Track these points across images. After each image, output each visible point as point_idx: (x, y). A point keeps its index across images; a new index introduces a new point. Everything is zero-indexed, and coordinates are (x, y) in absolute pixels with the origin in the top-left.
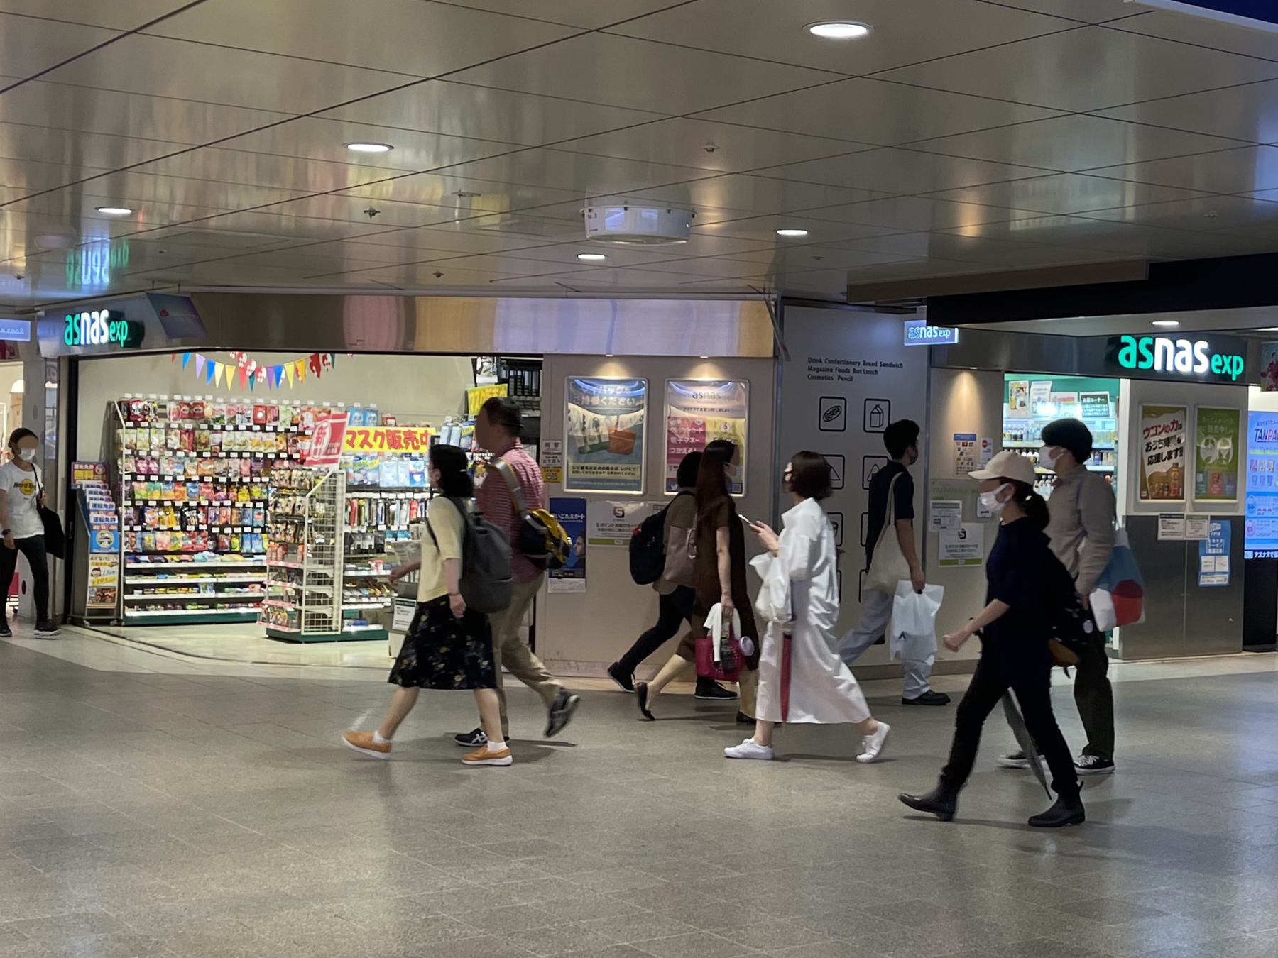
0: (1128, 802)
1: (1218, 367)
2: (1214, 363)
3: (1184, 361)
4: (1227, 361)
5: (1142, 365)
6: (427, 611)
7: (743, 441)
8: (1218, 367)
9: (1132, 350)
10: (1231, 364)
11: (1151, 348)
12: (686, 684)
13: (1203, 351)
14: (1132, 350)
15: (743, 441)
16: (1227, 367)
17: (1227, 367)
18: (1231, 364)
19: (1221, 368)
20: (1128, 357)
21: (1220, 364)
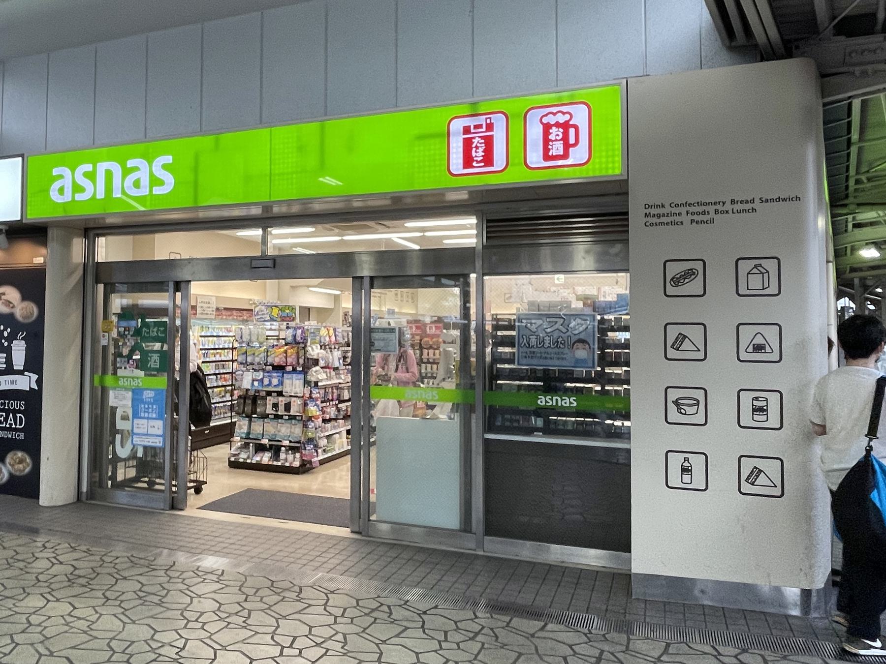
11: (91, 176)
20: (61, 190)
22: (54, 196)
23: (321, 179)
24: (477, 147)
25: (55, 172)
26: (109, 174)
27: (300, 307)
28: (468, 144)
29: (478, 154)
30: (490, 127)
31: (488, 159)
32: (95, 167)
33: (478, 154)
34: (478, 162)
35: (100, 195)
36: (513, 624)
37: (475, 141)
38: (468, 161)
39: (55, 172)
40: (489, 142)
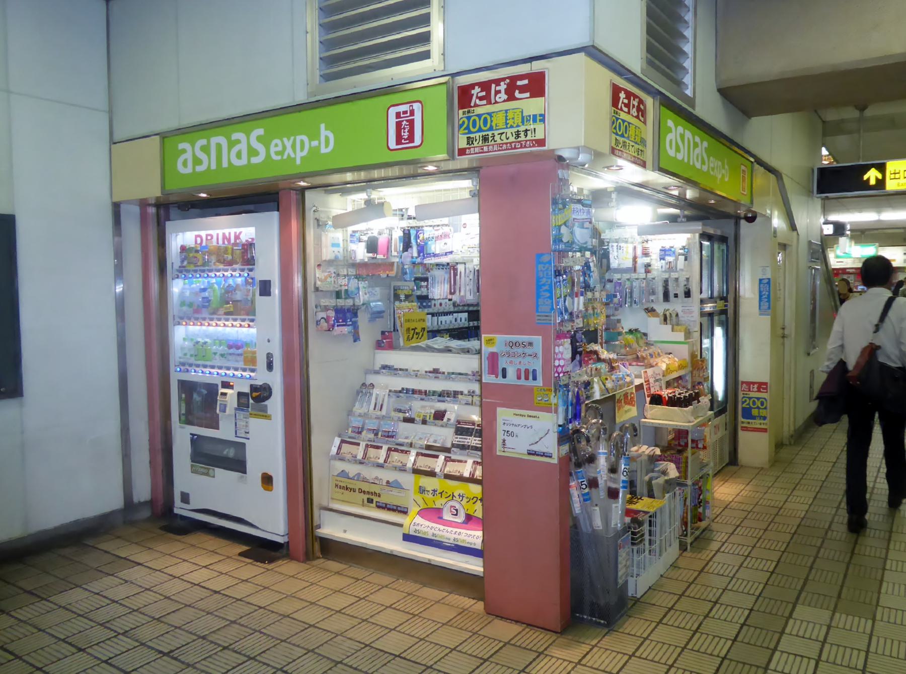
0: (268, 417)
1: (277, 153)
2: (273, 149)
3: (239, 155)
4: (288, 144)
5: (199, 169)
6: (895, 281)
7: (647, 405)
8: (277, 153)
9: (188, 156)
10: (293, 146)
11: (206, 149)
12: (471, 286)
13: (259, 139)
14: (188, 156)
15: (647, 405)
16: (289, 150)
17: (289, 150)
18: (293, 146)
19: (281, 153)
20: (185, 164)
21: (280, 148)
22: (180, 168)
23: (877, 415)
24: (404, 129)
25: (181, 146)
26: (219, 146)
27: (429, 32)
28: (399, 125)
29: (405, 134)
30: (412, 113)
31: (411, 138)
32: (209, 142)
33: (405, 134)
34: (405, 140)
35: (213, 166)
36: (446, 601)
37: (404, 123)
38: (399, 140)
39: (181, 146)
40: (411, 123)
